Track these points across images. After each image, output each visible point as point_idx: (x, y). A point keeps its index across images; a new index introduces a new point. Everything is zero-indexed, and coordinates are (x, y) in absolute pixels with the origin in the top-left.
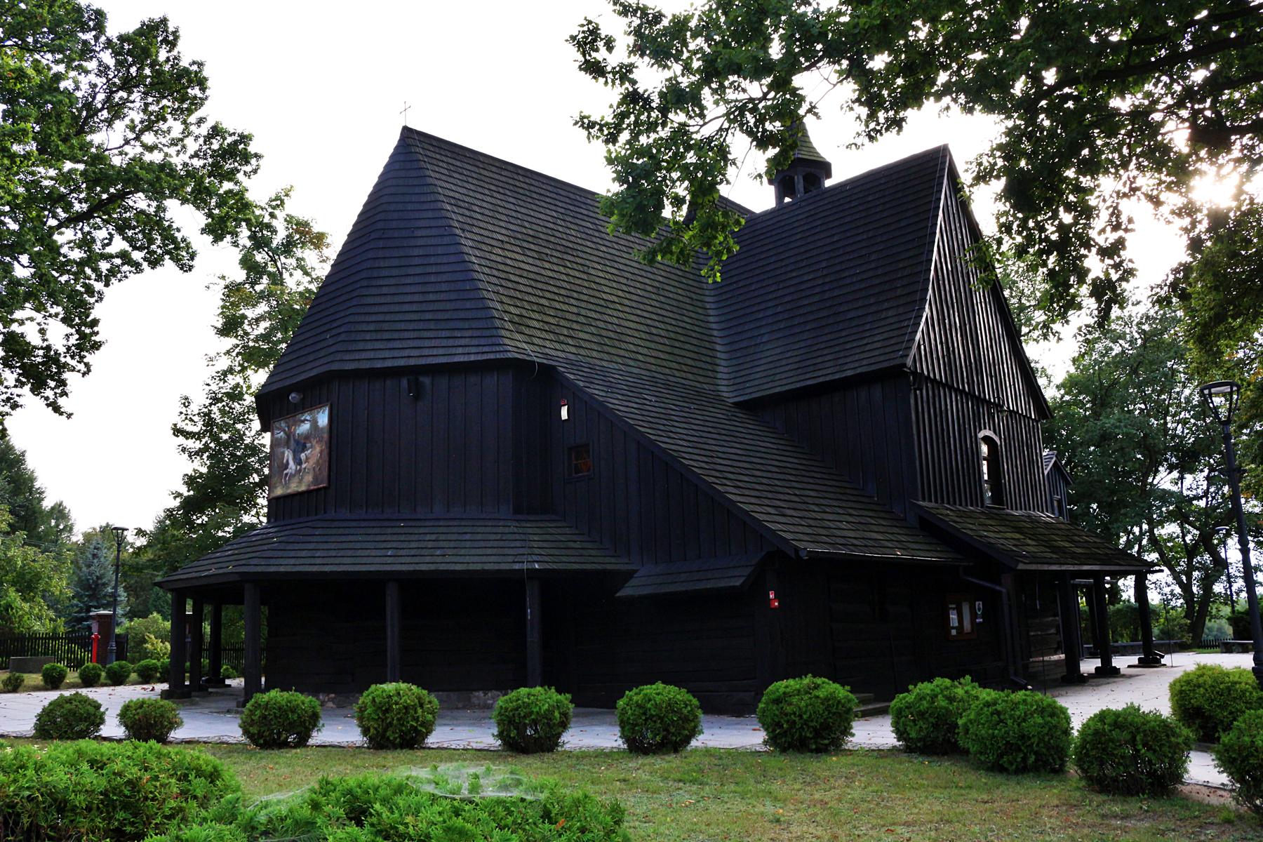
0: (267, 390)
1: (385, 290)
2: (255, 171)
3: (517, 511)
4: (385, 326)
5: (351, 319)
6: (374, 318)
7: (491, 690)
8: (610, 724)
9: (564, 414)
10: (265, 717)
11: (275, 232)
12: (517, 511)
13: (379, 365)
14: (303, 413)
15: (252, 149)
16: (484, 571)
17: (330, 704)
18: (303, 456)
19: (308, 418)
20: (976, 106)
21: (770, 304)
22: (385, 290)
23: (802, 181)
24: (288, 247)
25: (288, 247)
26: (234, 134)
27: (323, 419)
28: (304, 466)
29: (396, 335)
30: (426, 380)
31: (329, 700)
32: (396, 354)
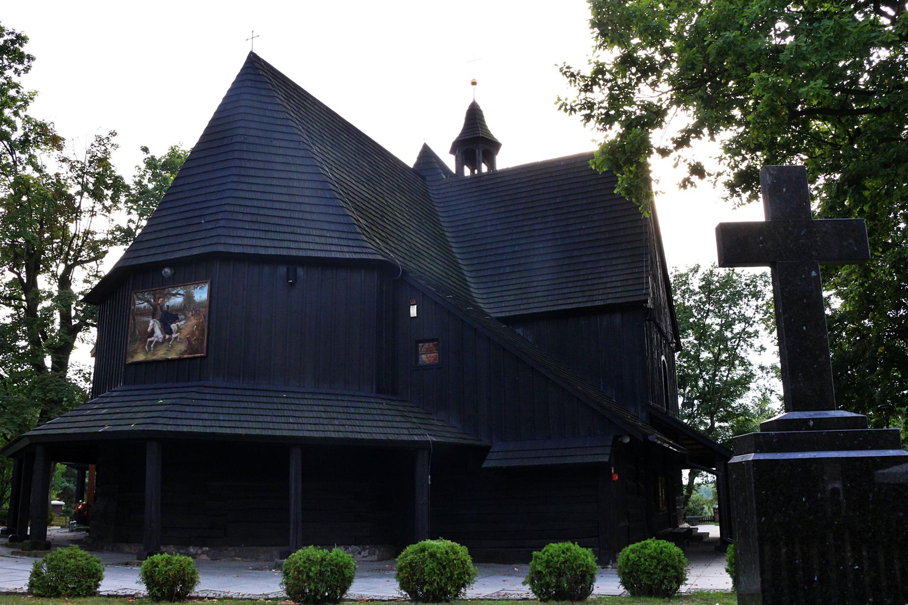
0: (119, 265)
1: (254, 188)
2: (26, 70)
3: (379, 391)
4: (261, 219)
5: (227, 208)
6: (248, 210)
7: (350, 545)
8: (613, 577)
9: (413, 311)
10: (321, 573)
11: (14, 128)
12: (379, 391)
13: (262, 252)
14: (174, 287)
15: (26, 49)
16: (326, 438)
17: (204, 557)
18: (174, 326)
19: (181, 292)
20: (32, 151)
21: (507, 244)
22: (254, 188)
23: (481, 155)
24: (24, 144)
25: (24, 144)
26: (13, 33)
27: (201, 294)
28: (174, 336)
29: (272, 228)
30: (301, 272)
31: (203, 553)
32: (277, 244)
